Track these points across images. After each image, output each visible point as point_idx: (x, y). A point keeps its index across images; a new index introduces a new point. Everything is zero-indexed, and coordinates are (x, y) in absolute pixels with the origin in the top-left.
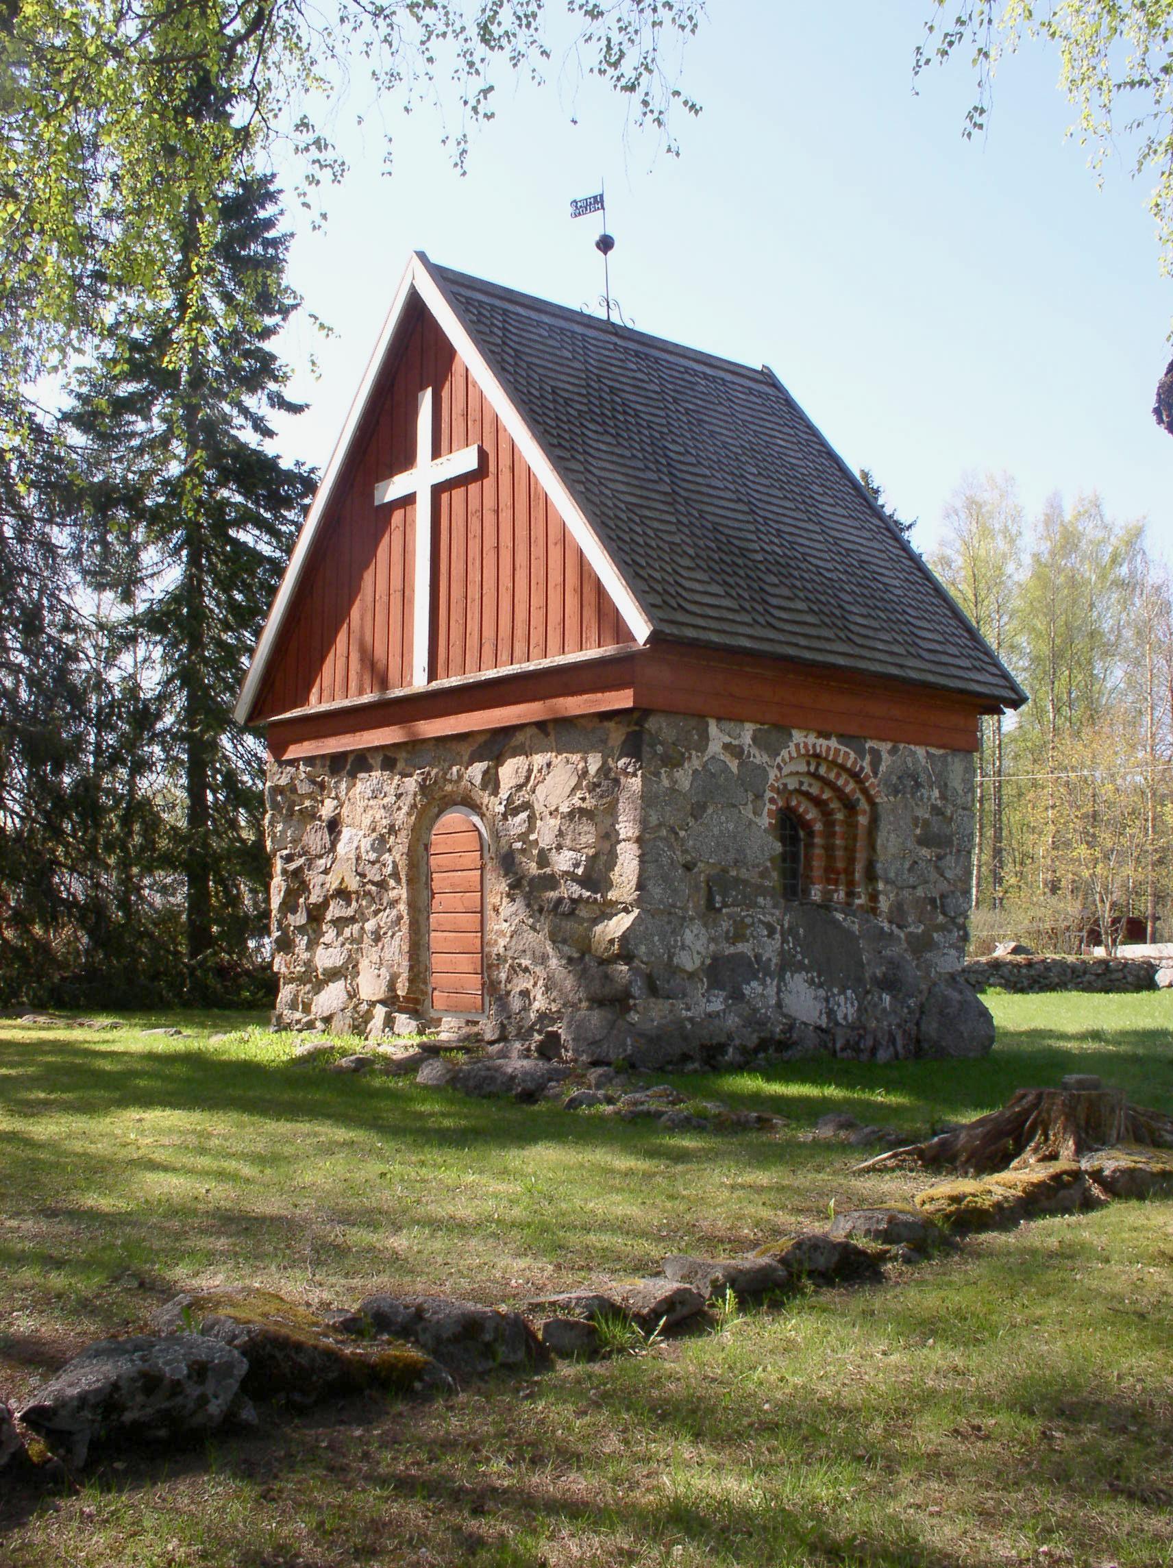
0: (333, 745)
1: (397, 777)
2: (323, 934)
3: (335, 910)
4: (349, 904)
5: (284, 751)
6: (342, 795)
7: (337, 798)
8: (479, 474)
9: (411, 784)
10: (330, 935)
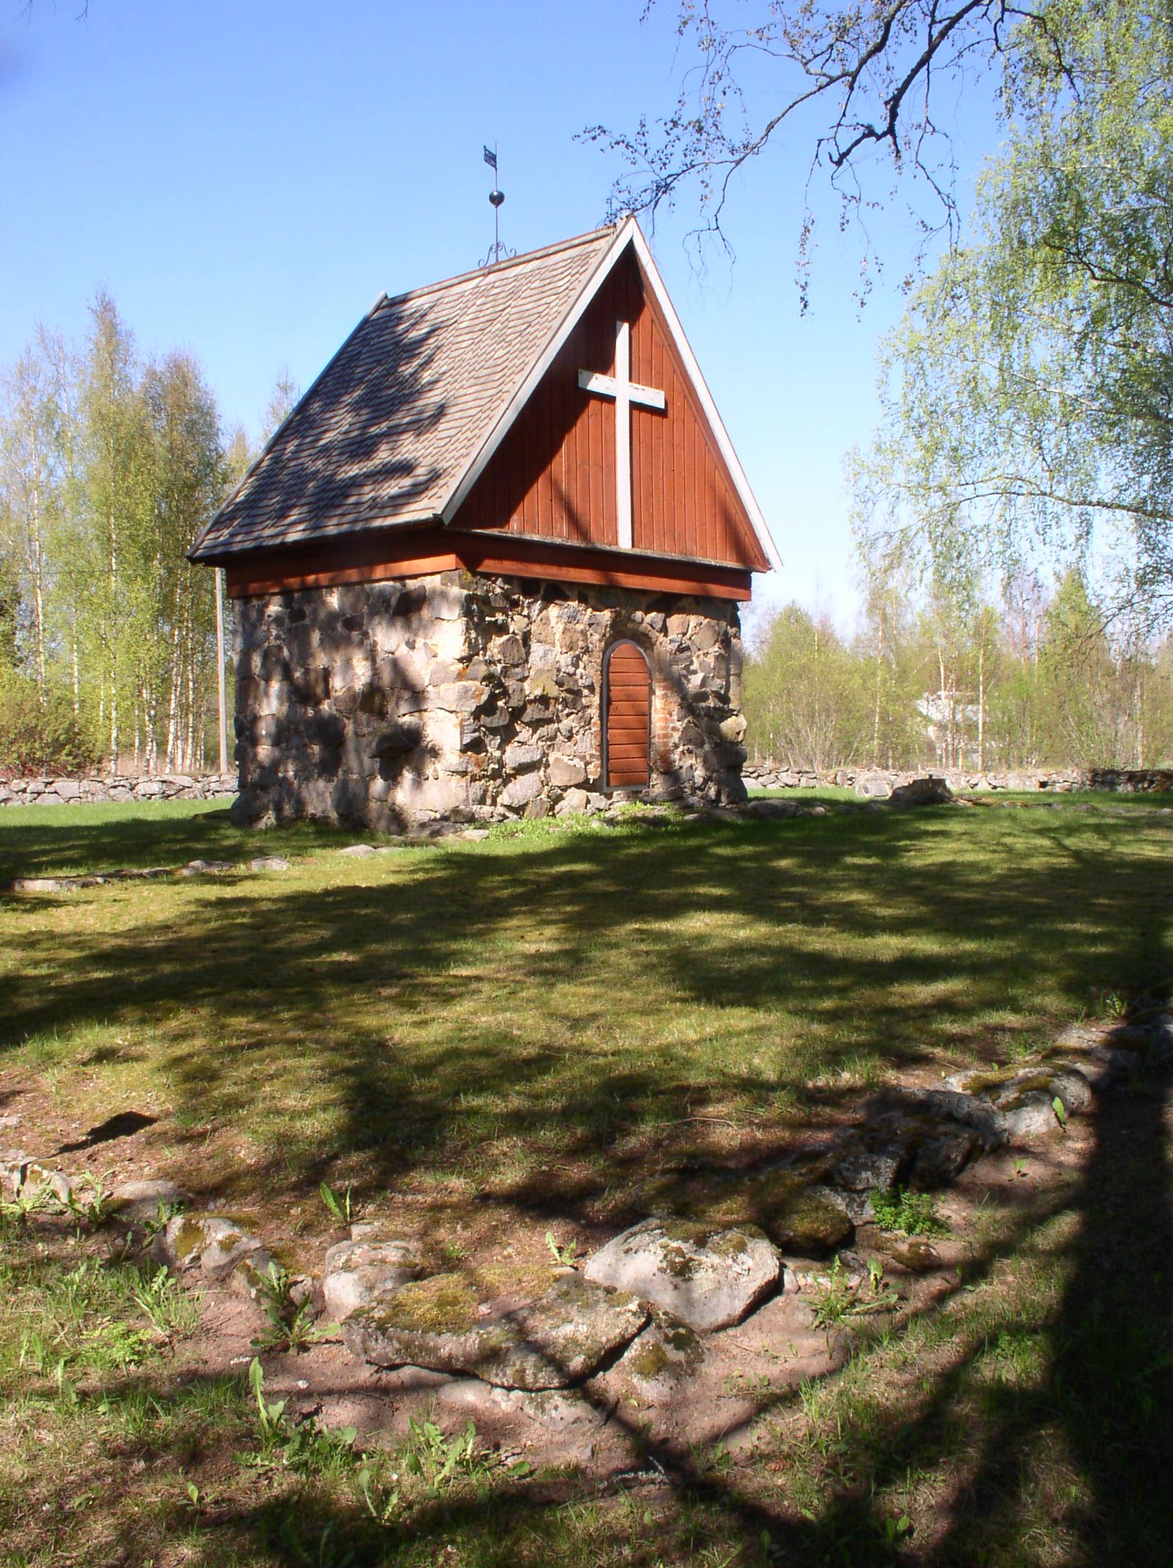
0: (537, 571)
1: (590, 610)
2: (517, 734)
3: (531, 713)
4: (547, 708)
5: (479, 563)
6: (534, 613)
7: (528, 616)
8: (661, 413)
9: (606, 616)
10: (524, 733)
